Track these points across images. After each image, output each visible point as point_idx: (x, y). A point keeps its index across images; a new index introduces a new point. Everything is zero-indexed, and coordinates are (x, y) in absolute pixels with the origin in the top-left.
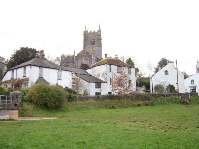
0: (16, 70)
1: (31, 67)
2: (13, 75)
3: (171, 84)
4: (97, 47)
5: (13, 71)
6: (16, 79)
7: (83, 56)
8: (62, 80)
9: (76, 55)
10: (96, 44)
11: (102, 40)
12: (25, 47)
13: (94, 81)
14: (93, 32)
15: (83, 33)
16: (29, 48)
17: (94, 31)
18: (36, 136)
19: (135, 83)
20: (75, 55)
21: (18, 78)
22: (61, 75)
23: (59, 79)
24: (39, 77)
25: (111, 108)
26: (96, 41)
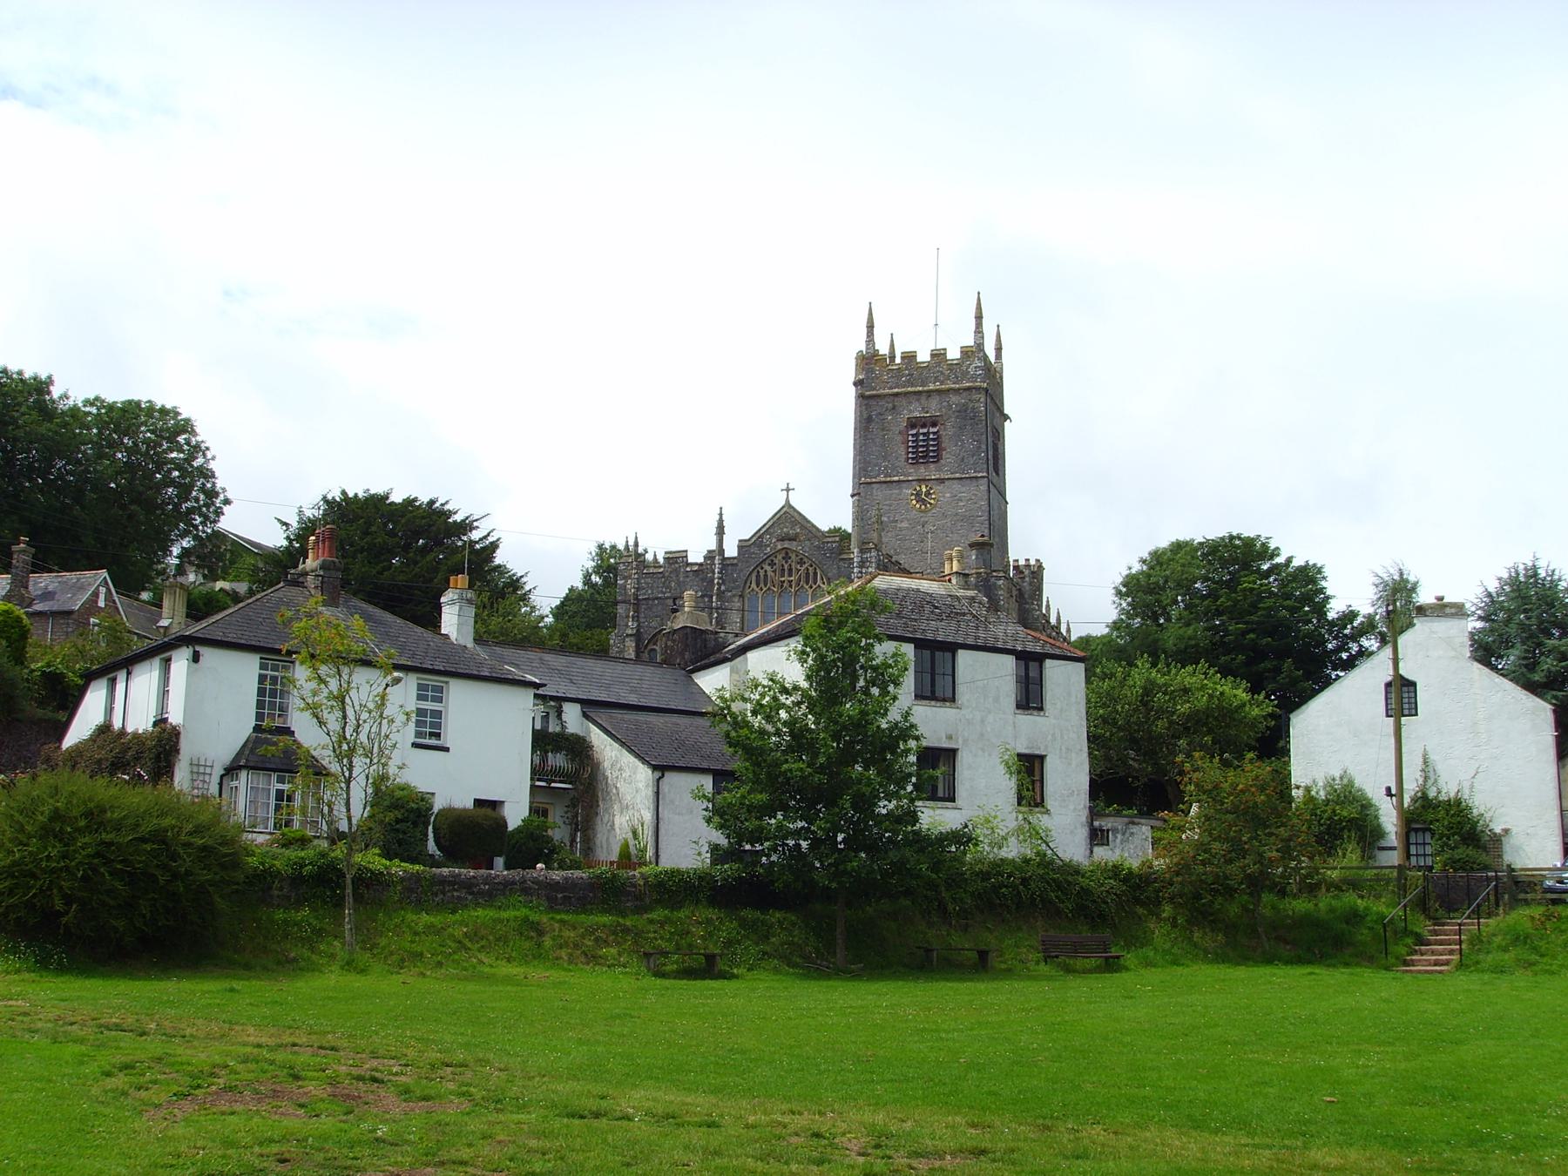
0: (156, 663)
1: (196, 658)
2: (109, 710)
3: (1448, 786)
4: (956, 486)
5: (113, 682)
6: (123, 732)
7: (787, 557)
8: (447, 750)
9: (731, 551)
10: (948, 457)
11: (1009, 429)
12: (357, 489)
13: (705, 765)
14: (924, 357)
15: (849, 373)
16: (397, 498)
17: (939, 355)
18: (301, 1046)
19: (1080, 779)
20: (721, 550)
21: (130, 729)
22: (437, 714)
23: (430, 735)
24: (257, 729)
25: (689, 973)
26: (948, 431)
